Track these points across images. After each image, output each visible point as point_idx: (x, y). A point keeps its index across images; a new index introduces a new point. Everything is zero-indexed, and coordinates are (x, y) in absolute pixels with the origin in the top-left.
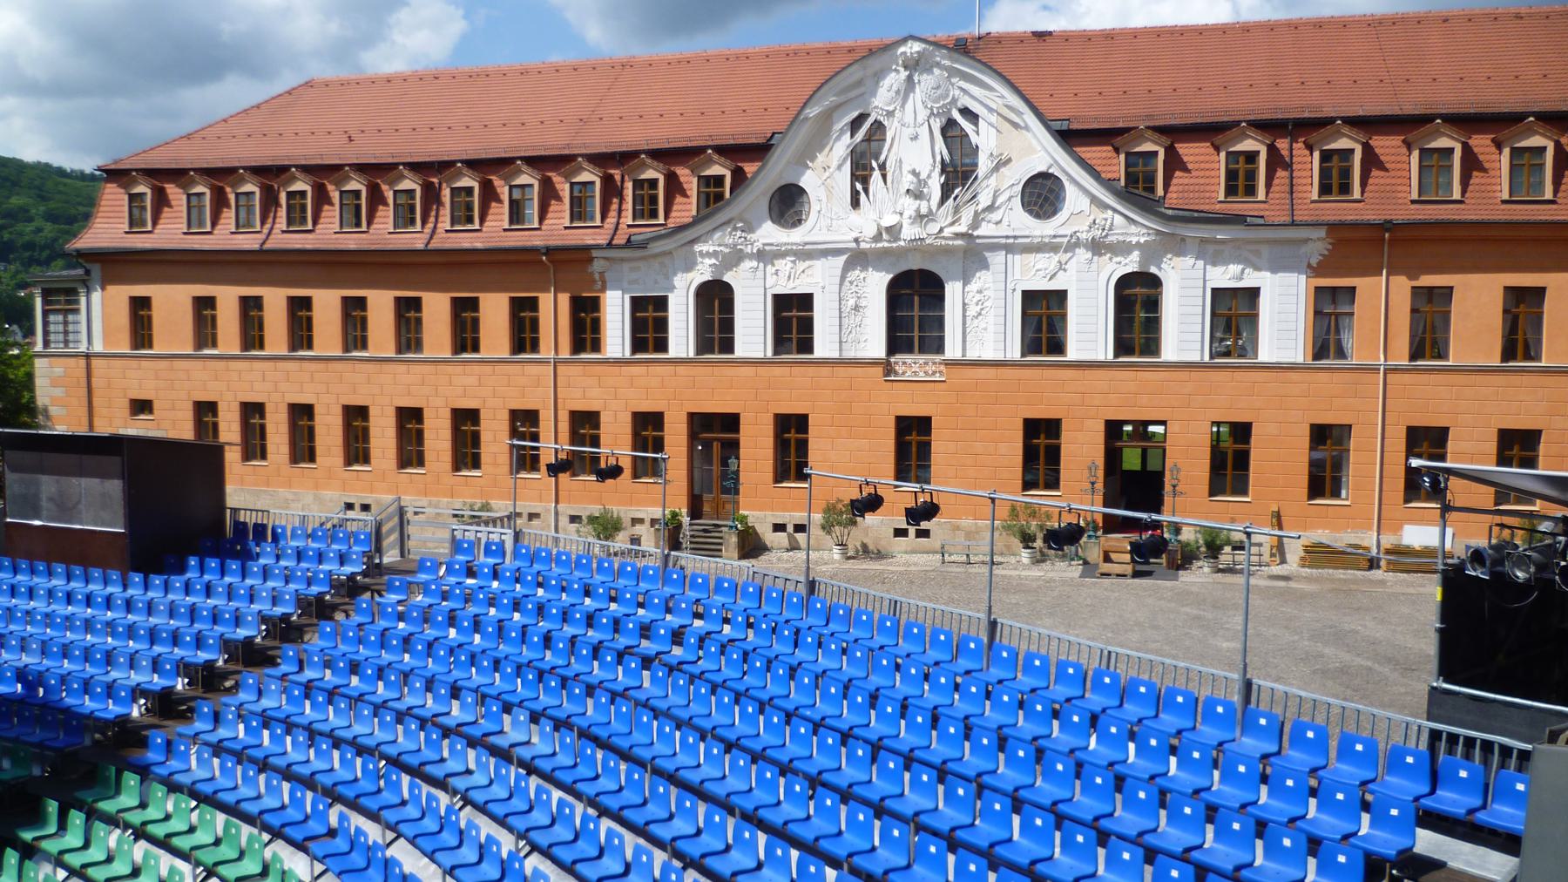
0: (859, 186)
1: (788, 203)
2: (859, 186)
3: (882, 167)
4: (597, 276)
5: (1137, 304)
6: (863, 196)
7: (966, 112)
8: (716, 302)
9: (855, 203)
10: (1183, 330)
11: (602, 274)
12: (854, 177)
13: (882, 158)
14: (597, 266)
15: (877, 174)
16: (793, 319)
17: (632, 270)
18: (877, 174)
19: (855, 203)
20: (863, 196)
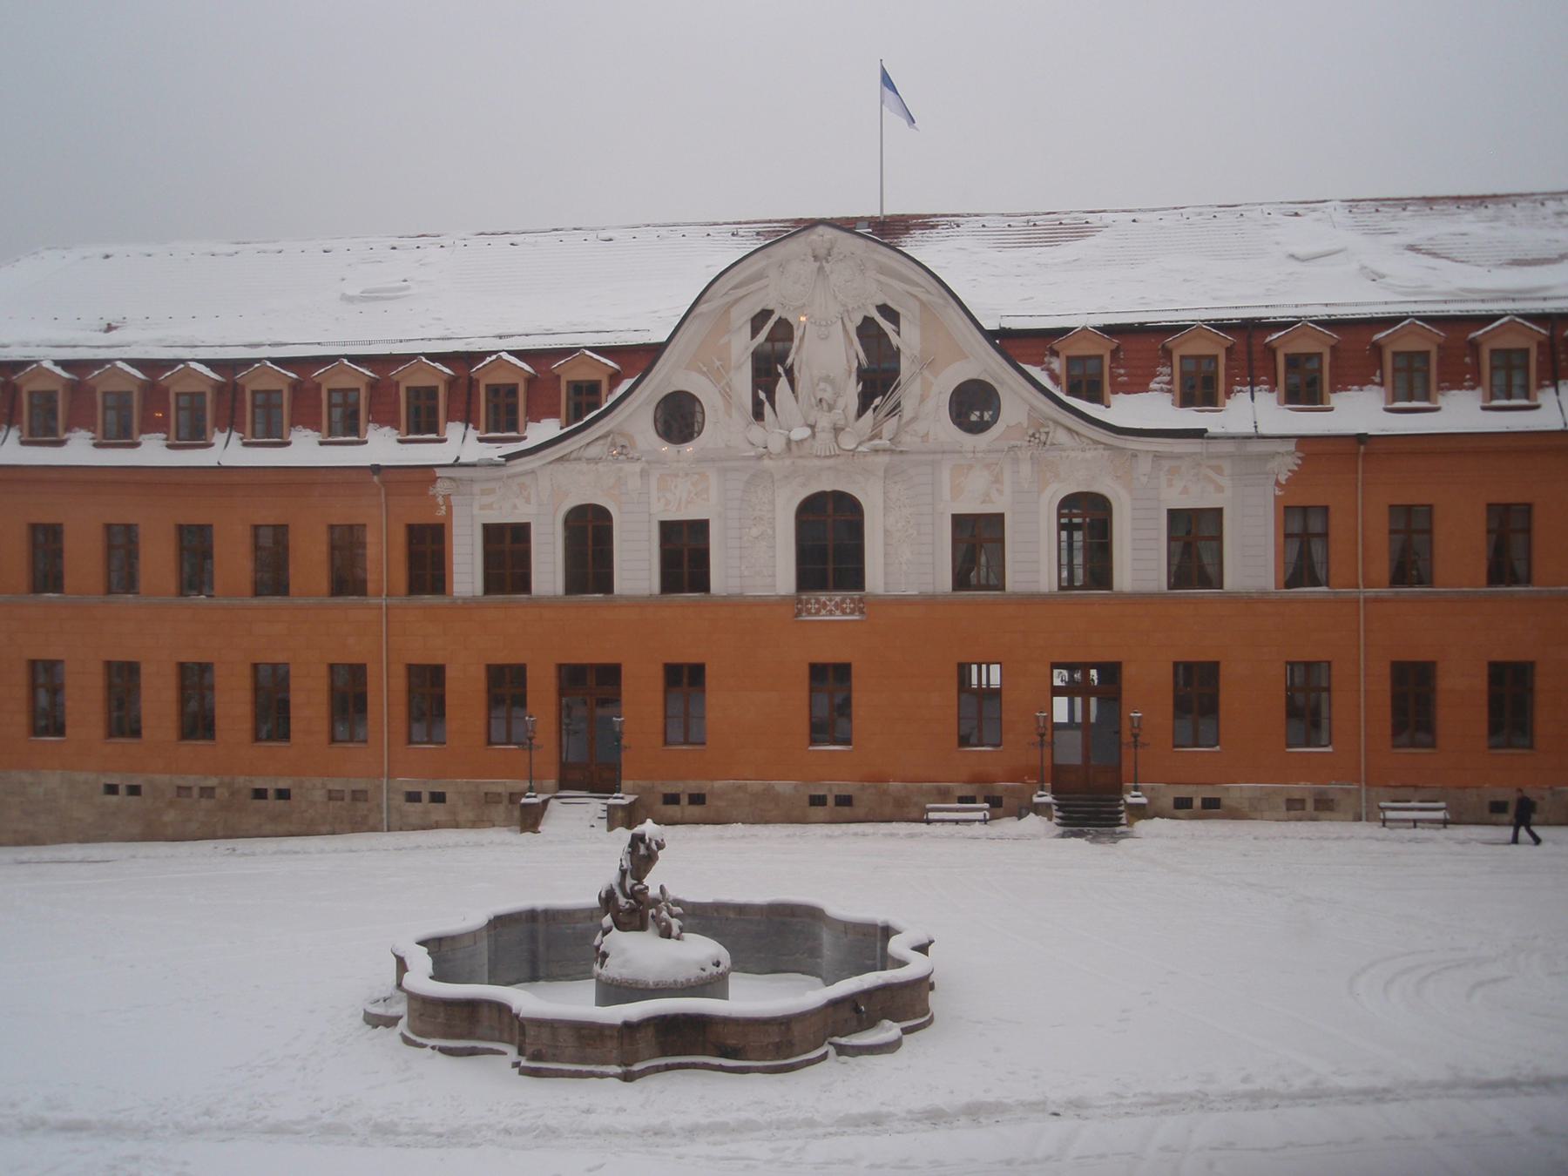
0: (762, 395)
1: (679, 418)
2: (762, 395)
3: (789, 372)
4: (440, 500)
5: (1087, 519)
6: (767, 406)
7: (884, 310)
8: (589, 533)
9: (758, 415)
10: (1140, 561)
11: (447, 497)
12: (756, 385)
13: (789, 361)
14: (441, 488)
15: (783, 382)
16: (685, 552)
17: (484, 492)
18: (783, 382)
19: (758, 415)
20: (767, 406)
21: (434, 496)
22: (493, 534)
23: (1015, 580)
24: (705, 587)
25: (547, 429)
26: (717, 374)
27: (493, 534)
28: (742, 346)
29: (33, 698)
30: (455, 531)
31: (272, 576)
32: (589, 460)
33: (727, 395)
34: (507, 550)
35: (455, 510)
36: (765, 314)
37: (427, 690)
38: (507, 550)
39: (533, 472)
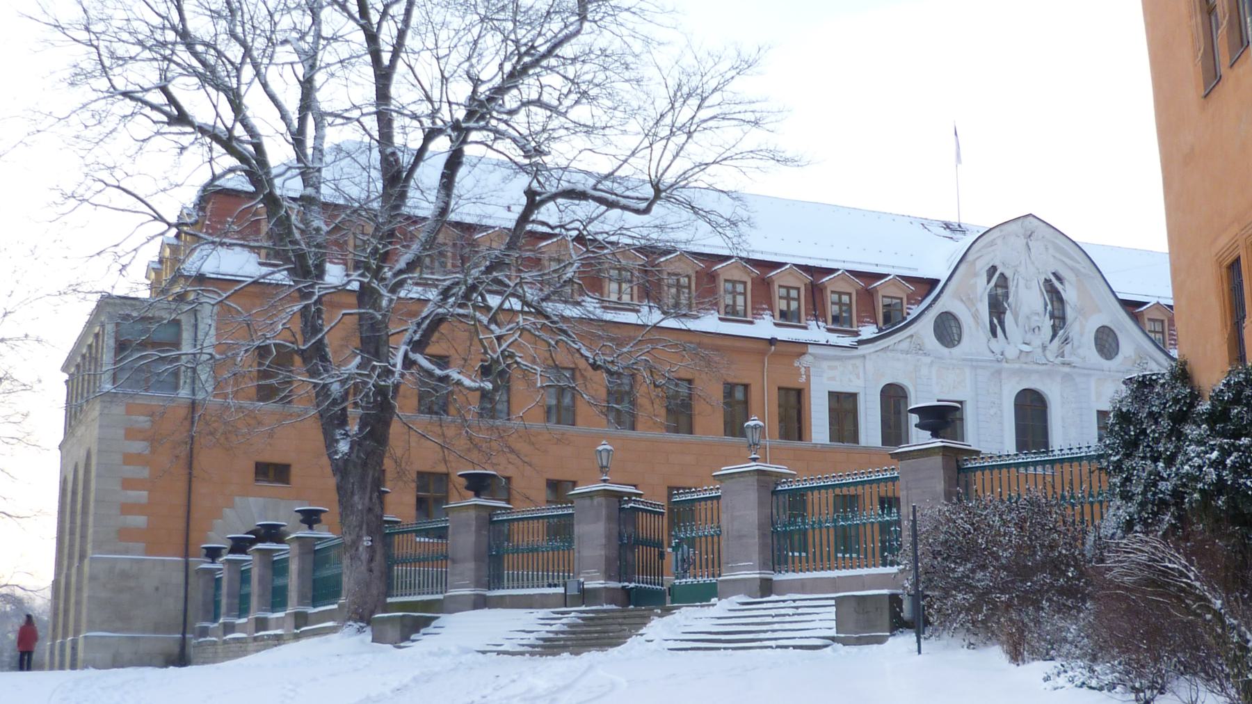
0: (995, 321)
2: (995, 321)
4: (803, 370)
6: (999, 328)
11: (808, 369)
14: (807, 360)
17: (830, 368)
20: (999, 328)
21: (799, 368)
22: (835, 397)
23: (863, 441)
24: (855, 439)
25: (868, 331)
26: (969, 302)
27: (835, 397)
28: (982, 288)
29: (279, 640)
30: (813, 394)
31: (681, 414)
32: (902, 352)
33: (976, 316)
34: (844, 408)
35: (812, 378)
36: (993, 269)
37: (681, 414)
38: (844, 408)
39: (864, 357)
